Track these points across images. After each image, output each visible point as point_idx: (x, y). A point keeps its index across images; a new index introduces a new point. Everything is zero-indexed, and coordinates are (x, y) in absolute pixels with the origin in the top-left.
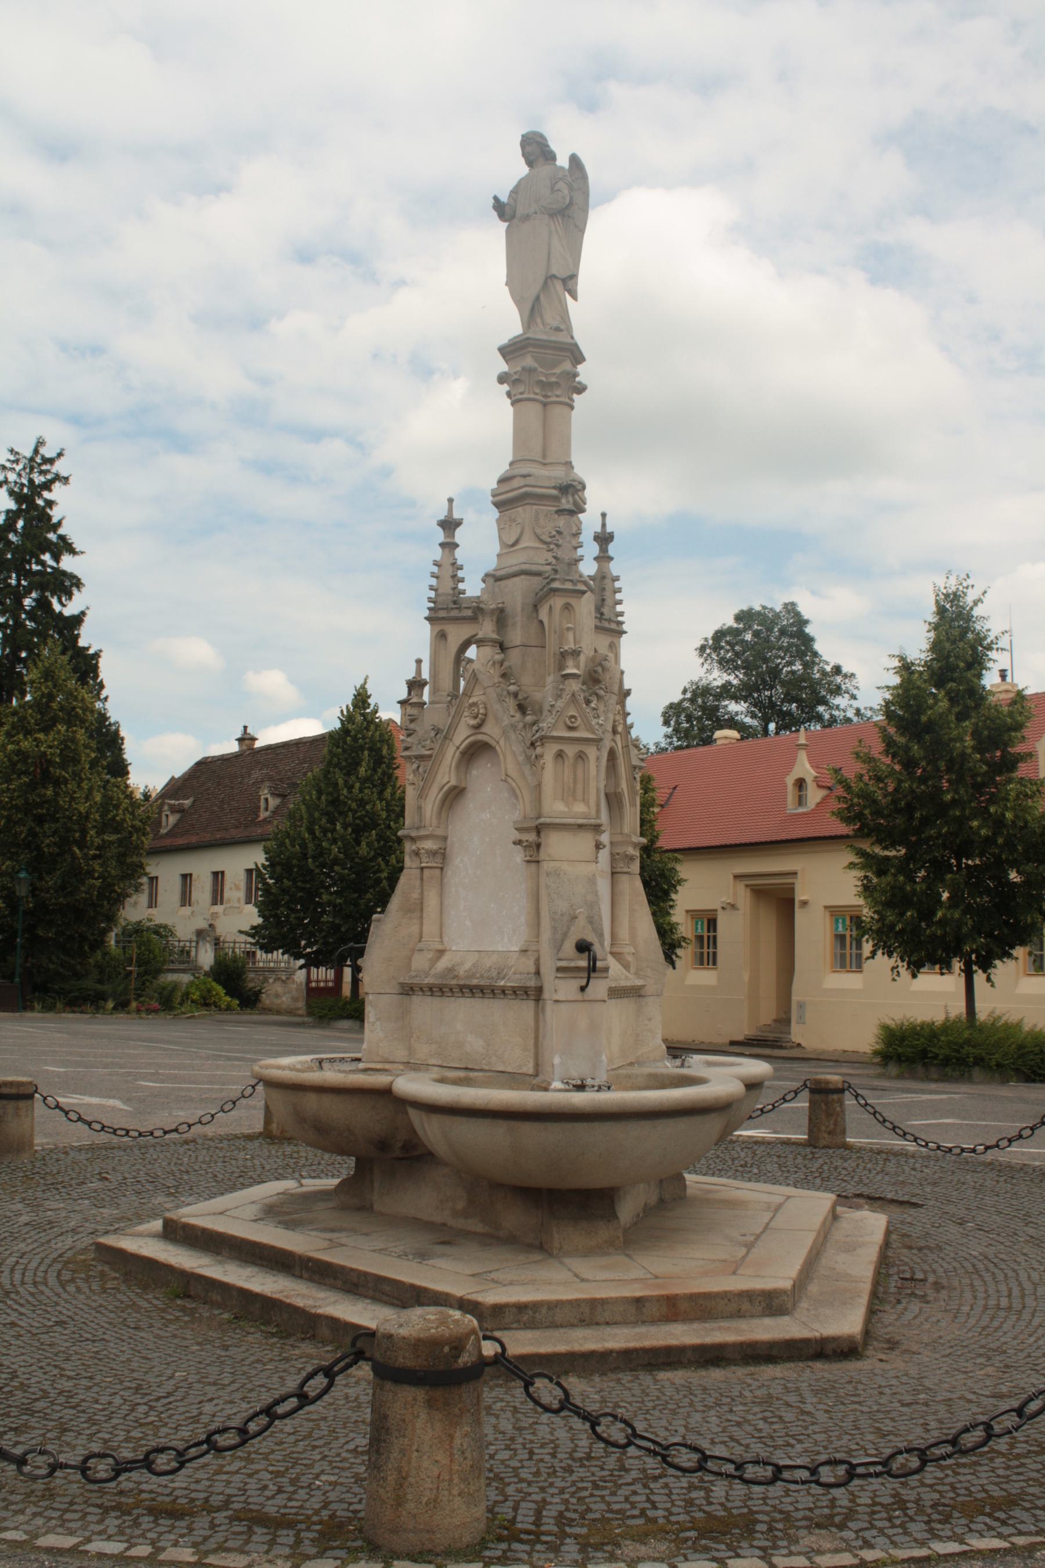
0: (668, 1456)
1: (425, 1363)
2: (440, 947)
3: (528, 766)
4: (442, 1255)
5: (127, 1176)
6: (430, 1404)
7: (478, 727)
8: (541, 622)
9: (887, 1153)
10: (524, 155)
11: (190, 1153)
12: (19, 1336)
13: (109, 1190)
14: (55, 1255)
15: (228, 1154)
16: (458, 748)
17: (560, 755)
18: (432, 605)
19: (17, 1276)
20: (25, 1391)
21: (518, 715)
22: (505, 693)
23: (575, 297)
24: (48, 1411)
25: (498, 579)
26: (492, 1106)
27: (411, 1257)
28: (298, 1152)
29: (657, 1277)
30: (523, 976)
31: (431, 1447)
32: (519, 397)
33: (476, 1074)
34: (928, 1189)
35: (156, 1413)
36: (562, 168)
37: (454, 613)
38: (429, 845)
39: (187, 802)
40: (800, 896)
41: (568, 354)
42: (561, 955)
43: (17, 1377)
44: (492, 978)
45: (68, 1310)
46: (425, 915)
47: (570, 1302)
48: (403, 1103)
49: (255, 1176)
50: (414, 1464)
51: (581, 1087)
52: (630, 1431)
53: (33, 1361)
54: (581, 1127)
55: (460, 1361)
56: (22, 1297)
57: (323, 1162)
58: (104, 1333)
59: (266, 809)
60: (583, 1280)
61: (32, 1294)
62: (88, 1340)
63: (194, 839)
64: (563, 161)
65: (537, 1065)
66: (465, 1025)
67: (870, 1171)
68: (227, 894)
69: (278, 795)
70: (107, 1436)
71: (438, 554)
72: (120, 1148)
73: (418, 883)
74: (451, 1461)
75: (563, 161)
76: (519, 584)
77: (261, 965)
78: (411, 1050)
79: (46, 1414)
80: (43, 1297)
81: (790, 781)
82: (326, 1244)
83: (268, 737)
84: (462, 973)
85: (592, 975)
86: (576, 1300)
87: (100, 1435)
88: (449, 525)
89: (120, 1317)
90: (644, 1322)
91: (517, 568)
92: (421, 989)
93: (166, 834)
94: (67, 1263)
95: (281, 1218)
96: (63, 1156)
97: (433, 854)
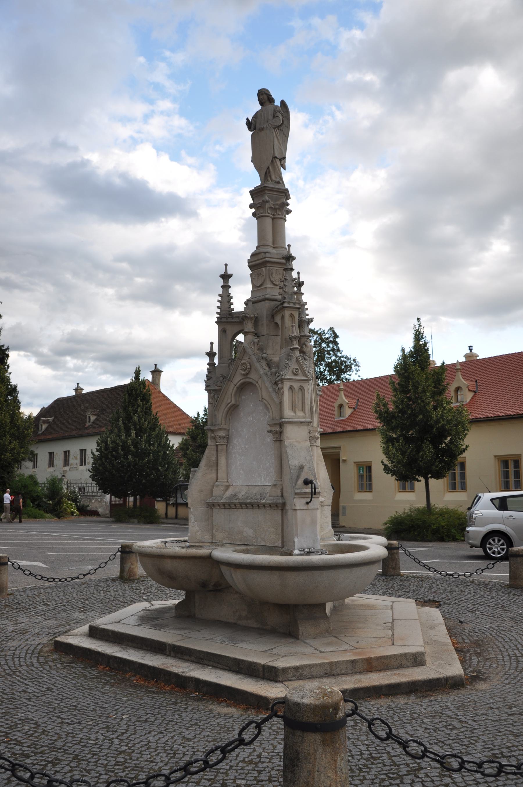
0: (445, 763)
1: (320, 719)
2: (227, 484)
3: (274, 393)
4: (243, 641)
5: (58, 602)
6: (324, 742)
7: (246, 375)
8: (277, 323)
9: (421, 578)
10: (259, 100)
11: (86, 589)
12: (30, 699)
13: (50, 610)
14: (32, 648)
15: (105, 589)
16: (235, 385)
17: (291, 388)
18: (218, 316)
19: (17, 662)
20: (47, 735)
21: (267, 368)
22: (260, 358)
23: (285, 169)
24: (65, 748)
25: (254, 303)
26: (272, 564)
27: (227, 643)
28: (139, 586)
29: (357, 648)
30: (275, 498)
31: (325, 768)
32: (261, 215)
33: (251, 547)
34: (449, 595)
35: (125, 744)
36: (277, 106)
37: (230, 320)
38: (222, 434)
39: (51, 419)
40: (342, 457)
41: (284, 195)
42: (297, 487)
43: (39, 726)
44: (258, 499)
45: (50, 680)
46: (219, 468)
47: (320, 665)
48: (218, 563)
49: (121, 600)
50: (316, 779)
51: (309, 553)
52: (423, 748)
53: (44, 714)
54: (317, 573)
55: (338, 716)
56: (23, 674)
57: (152, 591)
58: (75, 694)
59: (89, 421)
60: (321, 652)
61: (27, 672)
62: (67, 698)
63: (55, 436)
64: (277, 103)
65: (283, 542)
66: (242, 522)
67: (417, 586)
68: (71, 461)
69: (95, 415)
70: (105, 762)
71: (220, 291)
72: (50, 588)
73: (215, 453)
74: (336, 776)
75: (277, 103)
76: (267, 304)
77: (89, 494)
78: (213, 536)
79: (65, 750)
80: (34, 673)
81: (336, 405)
82: (180, 637)
83: (87, 389)
84: (240, 497)
85: (314, 496)
86: (323, 663)
87: (100, 762)
88: (226, 277)
89: (78, 683)
90: (356, 673)
91: (263, 297)
92: (219, 505)
93: (41, 434)
94: (39, 652)
95: (153, 623)
96: (22, 593)
97: (223, 437)
